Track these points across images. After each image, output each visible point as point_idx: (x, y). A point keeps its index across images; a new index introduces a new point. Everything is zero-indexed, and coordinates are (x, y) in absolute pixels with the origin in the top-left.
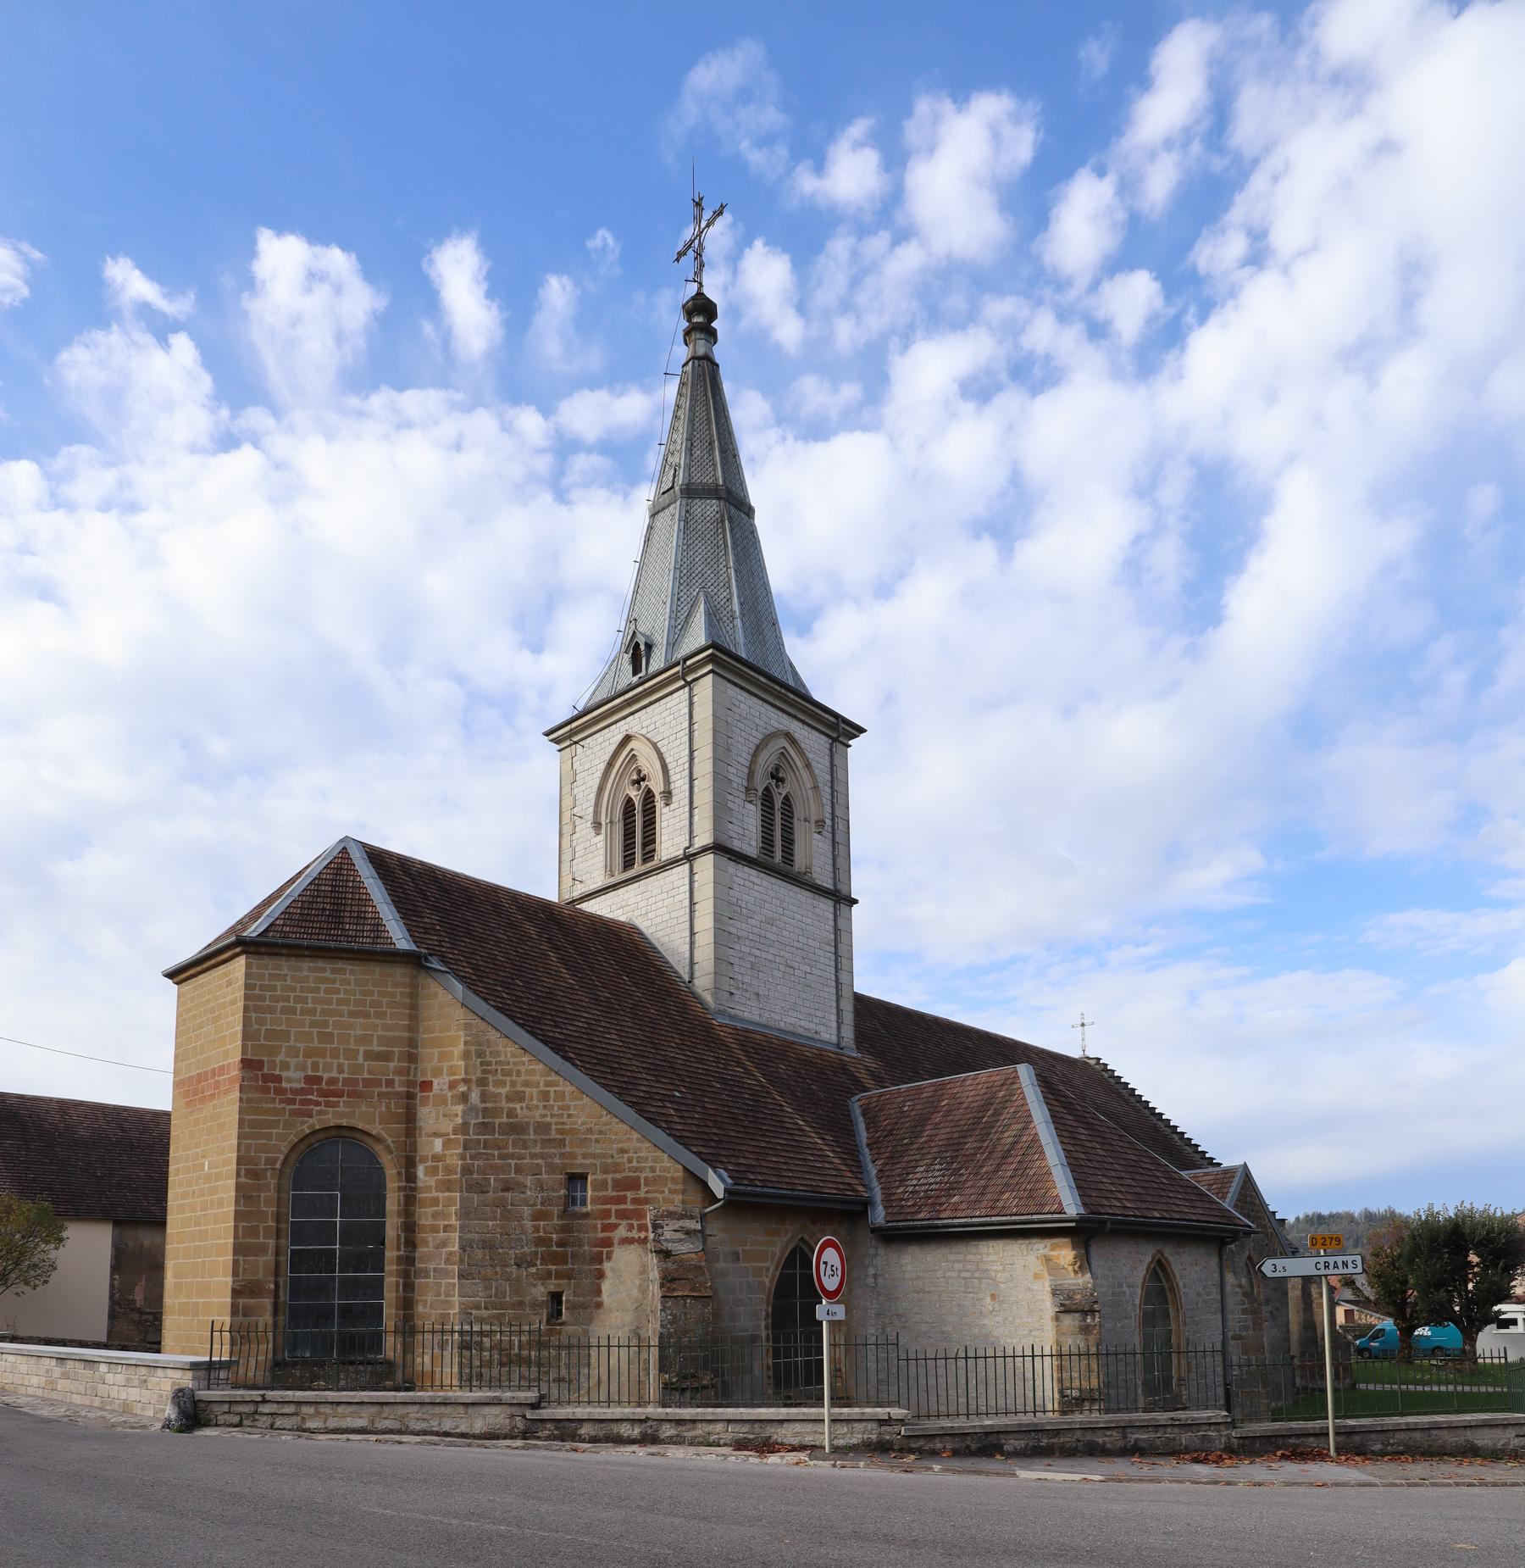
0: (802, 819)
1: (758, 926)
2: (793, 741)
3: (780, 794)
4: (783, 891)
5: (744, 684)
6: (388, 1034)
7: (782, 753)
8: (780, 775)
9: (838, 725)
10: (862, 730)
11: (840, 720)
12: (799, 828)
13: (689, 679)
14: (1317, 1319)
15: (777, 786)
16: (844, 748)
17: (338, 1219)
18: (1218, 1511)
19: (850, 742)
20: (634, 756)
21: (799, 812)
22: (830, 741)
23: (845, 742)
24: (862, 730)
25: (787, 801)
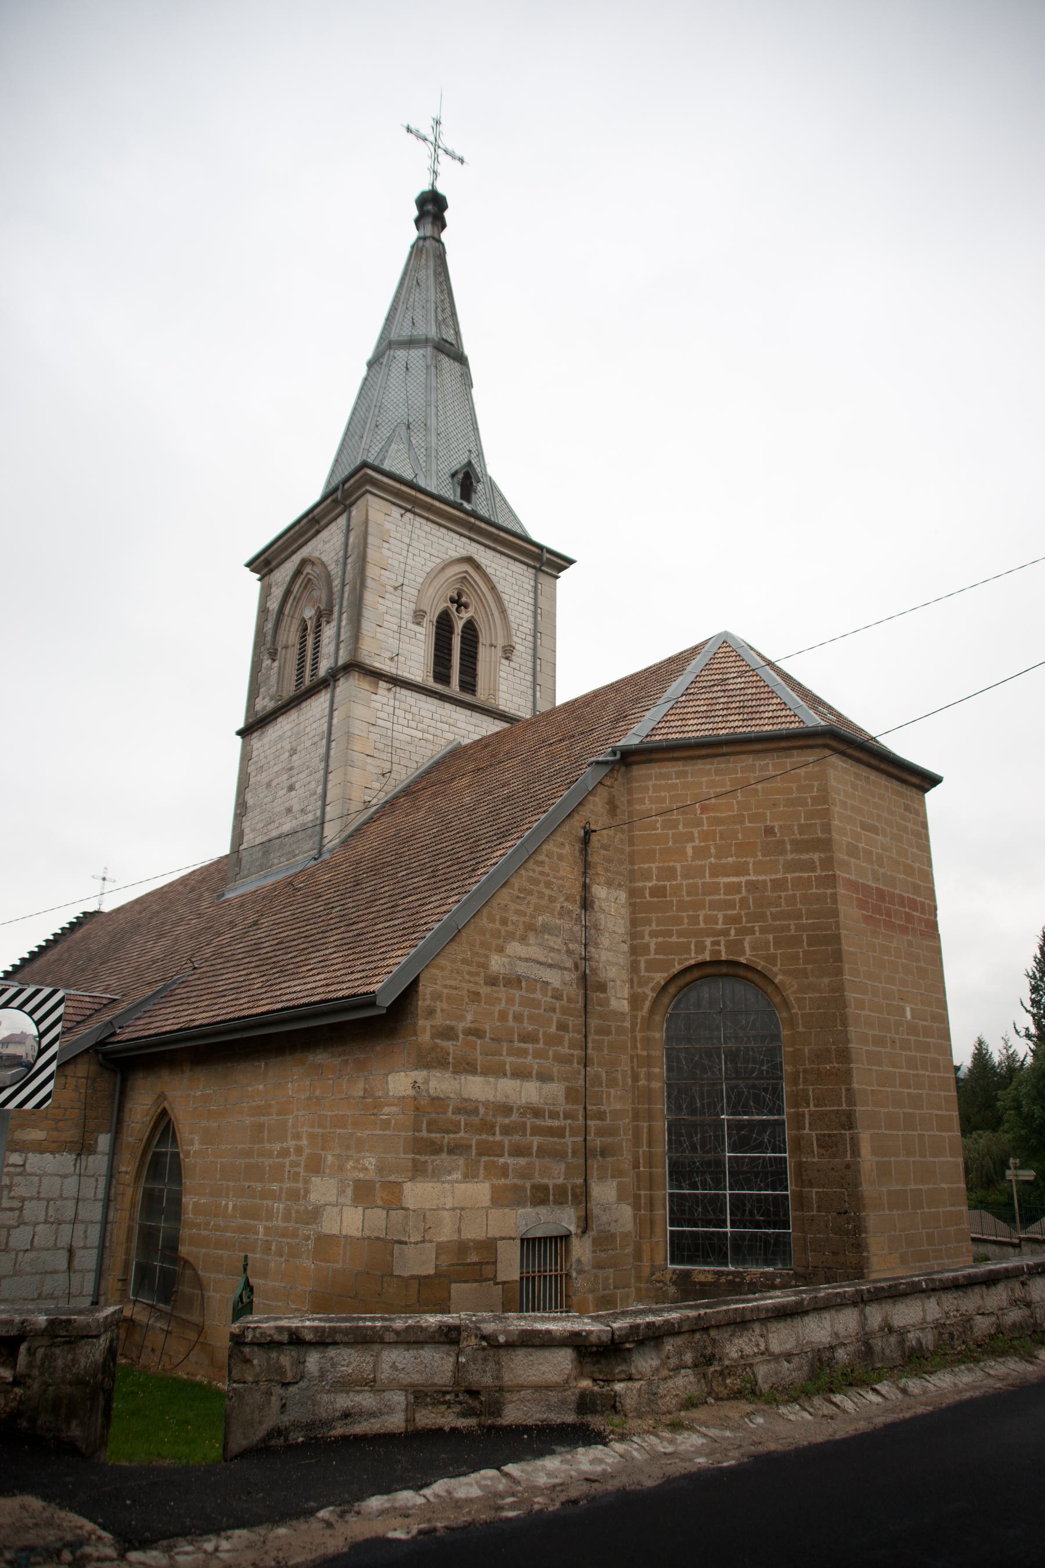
0: (488, 645)
1: (418, 748)
2: (477, 567)
3: (461, 618)
4: (412, 701)
5: (398, 502)
6: (894, 1132)
7: (465, 578)
8: (464, 599)
9: (541, 556)
10: (571, 562)
11: (545, 550)
12: (483, 654)
13: (348, 502)
14: (771, 1306)
15: (458, 610)
16: (551, 579)
17: (729, 1229)
18: (469, 1512)
19: (559, 574)
20: (310, 579)
21: (484, 638)
22: (533, 571)
23: (555, 573)
24: (571, 562)
25: (470, 628)
